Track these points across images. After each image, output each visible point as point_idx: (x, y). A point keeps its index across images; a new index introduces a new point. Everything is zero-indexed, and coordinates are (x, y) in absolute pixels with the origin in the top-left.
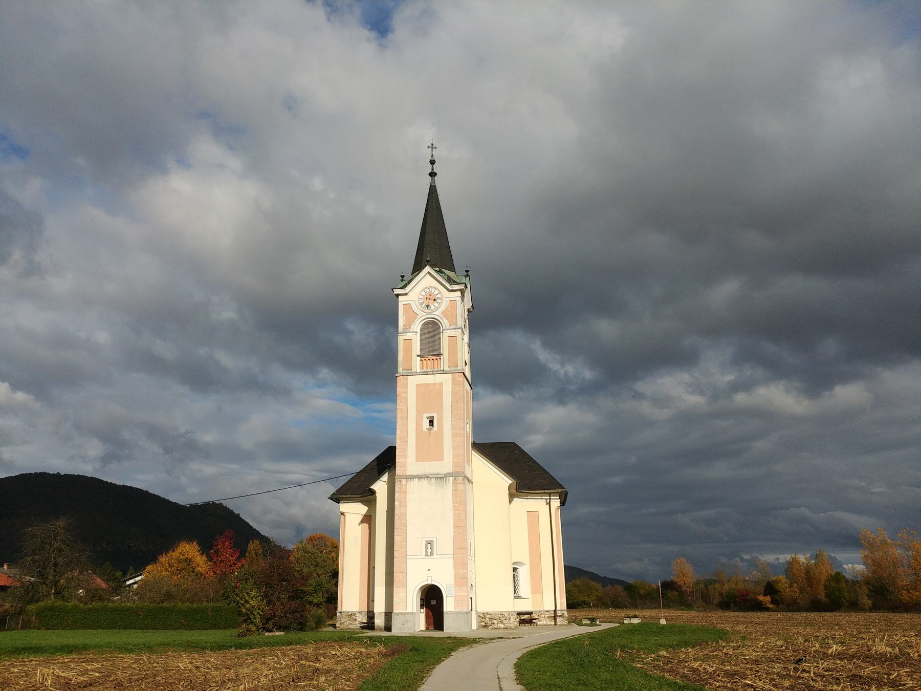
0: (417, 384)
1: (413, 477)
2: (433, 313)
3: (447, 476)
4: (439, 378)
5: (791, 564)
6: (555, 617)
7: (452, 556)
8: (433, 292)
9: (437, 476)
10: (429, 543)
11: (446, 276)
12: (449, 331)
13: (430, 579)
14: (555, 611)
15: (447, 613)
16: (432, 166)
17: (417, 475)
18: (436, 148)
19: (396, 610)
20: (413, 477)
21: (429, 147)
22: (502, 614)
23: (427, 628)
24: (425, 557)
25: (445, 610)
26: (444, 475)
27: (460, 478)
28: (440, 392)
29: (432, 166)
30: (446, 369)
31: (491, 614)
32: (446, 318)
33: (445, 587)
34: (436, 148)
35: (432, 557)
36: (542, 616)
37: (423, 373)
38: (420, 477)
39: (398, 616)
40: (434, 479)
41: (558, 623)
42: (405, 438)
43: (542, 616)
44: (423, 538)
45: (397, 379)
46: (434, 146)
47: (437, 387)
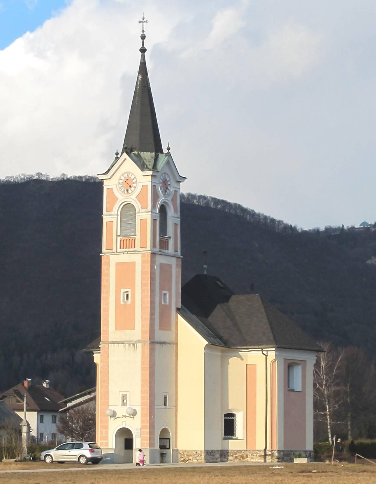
0: (116, 263)
1: (114, 343)
3: (138, 342)
5: (21, 400)
6: (265, 455)
7: (156, 407)
8: (130, 177)
10: (124, 397)
13: (124, 423)
14: (265, 450)
16: (143, 42)
18: (147, 22)
20: (114, 343)
21: (140, 22)
22: (197, 452)
26: (135, 341)
29: (143, 42)
31: (188, 452)
32: (140, 202)
34: (147, 22)
36: (254, 455)
41: (267, 461)
43: (254, 455)
44: (128, 392)
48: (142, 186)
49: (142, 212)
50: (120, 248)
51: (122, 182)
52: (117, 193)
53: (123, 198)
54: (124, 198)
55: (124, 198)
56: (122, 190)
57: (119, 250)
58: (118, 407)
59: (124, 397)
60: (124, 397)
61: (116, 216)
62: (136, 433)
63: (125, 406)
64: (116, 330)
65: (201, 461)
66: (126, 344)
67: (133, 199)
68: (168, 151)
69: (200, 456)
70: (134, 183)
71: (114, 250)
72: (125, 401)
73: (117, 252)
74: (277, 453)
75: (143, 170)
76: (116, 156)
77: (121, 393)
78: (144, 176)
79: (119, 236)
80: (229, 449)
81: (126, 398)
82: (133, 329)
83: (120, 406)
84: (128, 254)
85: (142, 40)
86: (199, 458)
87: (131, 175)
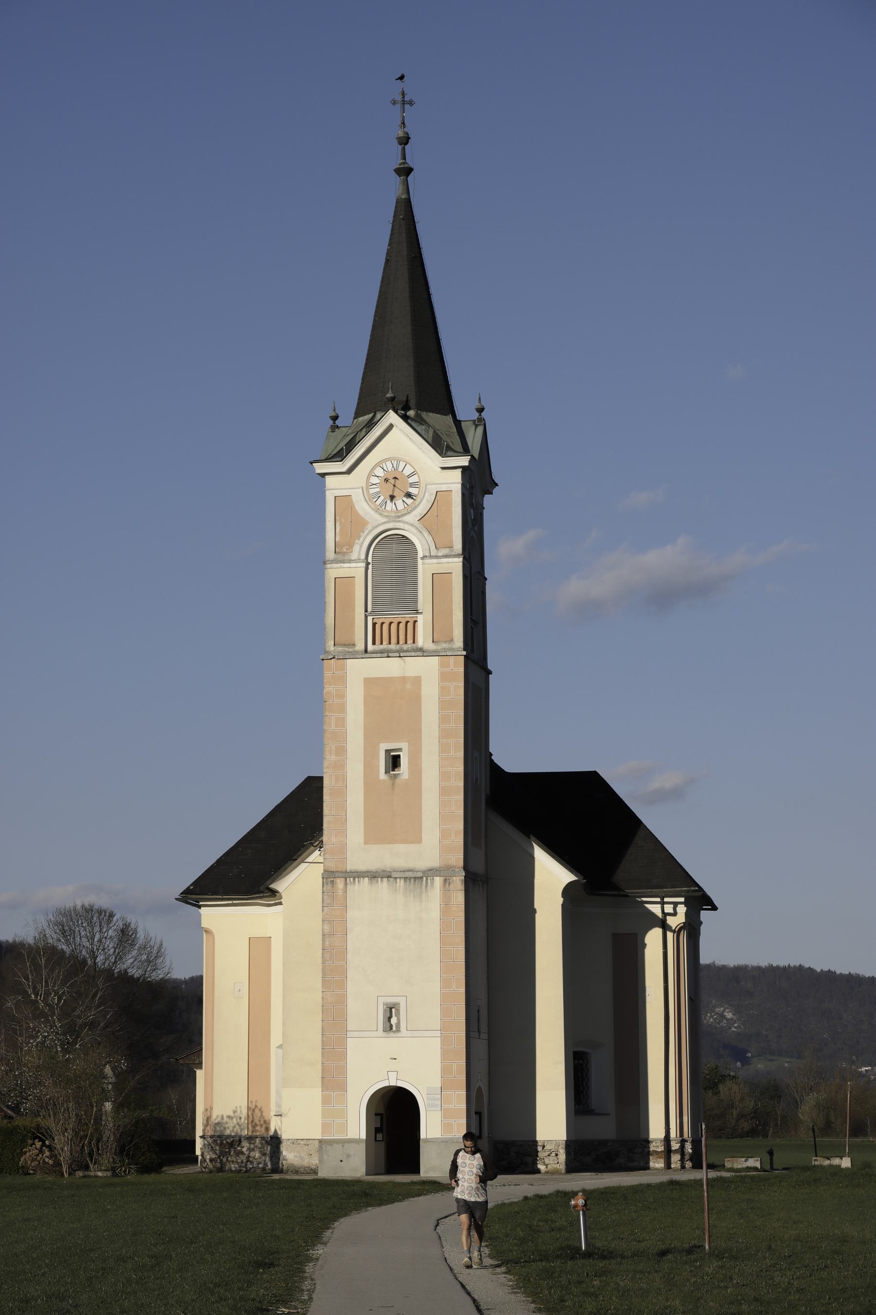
1: (358, 875)
2: (401, 519)
3: (430, 873)
4: (414, 666)
7: (438, 1034)
8: (400, 469)
9: (408, 874)
10: (391, 1010)
11: (431, 431)
12: (435, 561)
13: (393, 1076)
15: (427, 1141)
16: (404, 150)
17: (368, 872)
18: (411, 103)
19: (411, 522)
20: (358, 875)
21: (394, 103)
23: (367, 1174)
24: (384, 1034)
25: (423, 1136)
26: (424, 872)
27: (454, 878)
28: (416, 699)
29: (404, 150)
30: (430, 646)
33: (424, 1095)
34: (411, 103)
35: (398, 1035)
37: (379, 655)
38: (373, 876)
39: (331, 1145)
40: (402, 881)
41: (672, 1166)
42: (341, 766)
45: (324, 485)
46: (406, 99)
47: (408, 686)
48: (437, 493)
49: (437, 557)
50: (374, 643)
51: (379, 481)
52: (363, 508)
53: (382, 520)
54: (385, 520)
55: (385, 520)
56: (378, 503)
57: (370, 647)
58: (375, 1034)
59: (391, 1010)
60: (391, 1009)
61: (364, 565)
62: (428, 1099)
63: (394, 1032)
64: (365, 843)
65: (558, 1166)
66: (396, 878)
67: (412, 525)
68: (478, 414)
69: (553, 1154)
70: (412, 485)
71: (360, 646)
72: (394, 1021)
73: (366, 651)
74: (691, 1147)
75: (442, 454)
76: (331, 422)
77: (382, 1000)
78: (443, 468)
79: (371, 614)
80: (649, 1138)
81: (398, 1011)
82: (418, 840)
83: (380, 1032)
84: (400, 657)
85: (400, 147)
86: (553, 1161)
87: (402, 465)
